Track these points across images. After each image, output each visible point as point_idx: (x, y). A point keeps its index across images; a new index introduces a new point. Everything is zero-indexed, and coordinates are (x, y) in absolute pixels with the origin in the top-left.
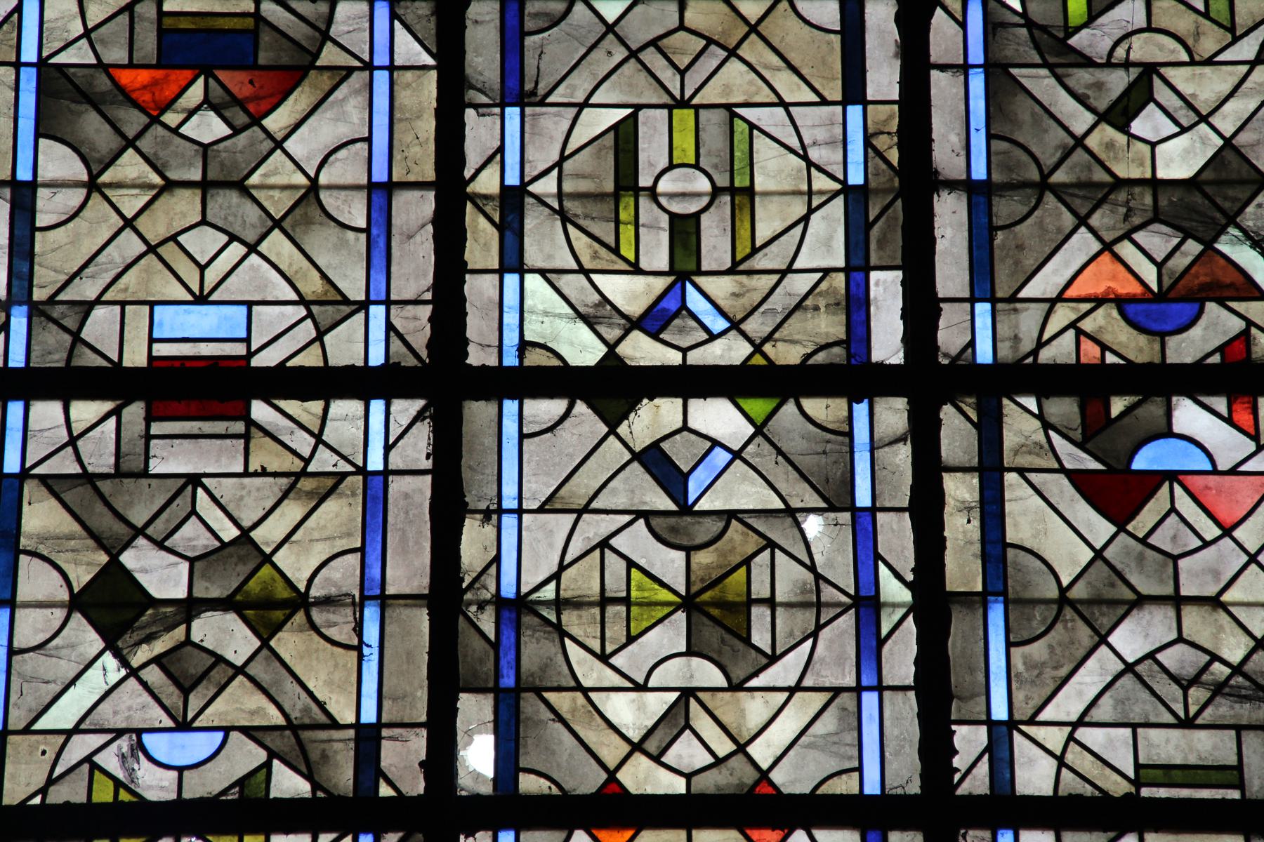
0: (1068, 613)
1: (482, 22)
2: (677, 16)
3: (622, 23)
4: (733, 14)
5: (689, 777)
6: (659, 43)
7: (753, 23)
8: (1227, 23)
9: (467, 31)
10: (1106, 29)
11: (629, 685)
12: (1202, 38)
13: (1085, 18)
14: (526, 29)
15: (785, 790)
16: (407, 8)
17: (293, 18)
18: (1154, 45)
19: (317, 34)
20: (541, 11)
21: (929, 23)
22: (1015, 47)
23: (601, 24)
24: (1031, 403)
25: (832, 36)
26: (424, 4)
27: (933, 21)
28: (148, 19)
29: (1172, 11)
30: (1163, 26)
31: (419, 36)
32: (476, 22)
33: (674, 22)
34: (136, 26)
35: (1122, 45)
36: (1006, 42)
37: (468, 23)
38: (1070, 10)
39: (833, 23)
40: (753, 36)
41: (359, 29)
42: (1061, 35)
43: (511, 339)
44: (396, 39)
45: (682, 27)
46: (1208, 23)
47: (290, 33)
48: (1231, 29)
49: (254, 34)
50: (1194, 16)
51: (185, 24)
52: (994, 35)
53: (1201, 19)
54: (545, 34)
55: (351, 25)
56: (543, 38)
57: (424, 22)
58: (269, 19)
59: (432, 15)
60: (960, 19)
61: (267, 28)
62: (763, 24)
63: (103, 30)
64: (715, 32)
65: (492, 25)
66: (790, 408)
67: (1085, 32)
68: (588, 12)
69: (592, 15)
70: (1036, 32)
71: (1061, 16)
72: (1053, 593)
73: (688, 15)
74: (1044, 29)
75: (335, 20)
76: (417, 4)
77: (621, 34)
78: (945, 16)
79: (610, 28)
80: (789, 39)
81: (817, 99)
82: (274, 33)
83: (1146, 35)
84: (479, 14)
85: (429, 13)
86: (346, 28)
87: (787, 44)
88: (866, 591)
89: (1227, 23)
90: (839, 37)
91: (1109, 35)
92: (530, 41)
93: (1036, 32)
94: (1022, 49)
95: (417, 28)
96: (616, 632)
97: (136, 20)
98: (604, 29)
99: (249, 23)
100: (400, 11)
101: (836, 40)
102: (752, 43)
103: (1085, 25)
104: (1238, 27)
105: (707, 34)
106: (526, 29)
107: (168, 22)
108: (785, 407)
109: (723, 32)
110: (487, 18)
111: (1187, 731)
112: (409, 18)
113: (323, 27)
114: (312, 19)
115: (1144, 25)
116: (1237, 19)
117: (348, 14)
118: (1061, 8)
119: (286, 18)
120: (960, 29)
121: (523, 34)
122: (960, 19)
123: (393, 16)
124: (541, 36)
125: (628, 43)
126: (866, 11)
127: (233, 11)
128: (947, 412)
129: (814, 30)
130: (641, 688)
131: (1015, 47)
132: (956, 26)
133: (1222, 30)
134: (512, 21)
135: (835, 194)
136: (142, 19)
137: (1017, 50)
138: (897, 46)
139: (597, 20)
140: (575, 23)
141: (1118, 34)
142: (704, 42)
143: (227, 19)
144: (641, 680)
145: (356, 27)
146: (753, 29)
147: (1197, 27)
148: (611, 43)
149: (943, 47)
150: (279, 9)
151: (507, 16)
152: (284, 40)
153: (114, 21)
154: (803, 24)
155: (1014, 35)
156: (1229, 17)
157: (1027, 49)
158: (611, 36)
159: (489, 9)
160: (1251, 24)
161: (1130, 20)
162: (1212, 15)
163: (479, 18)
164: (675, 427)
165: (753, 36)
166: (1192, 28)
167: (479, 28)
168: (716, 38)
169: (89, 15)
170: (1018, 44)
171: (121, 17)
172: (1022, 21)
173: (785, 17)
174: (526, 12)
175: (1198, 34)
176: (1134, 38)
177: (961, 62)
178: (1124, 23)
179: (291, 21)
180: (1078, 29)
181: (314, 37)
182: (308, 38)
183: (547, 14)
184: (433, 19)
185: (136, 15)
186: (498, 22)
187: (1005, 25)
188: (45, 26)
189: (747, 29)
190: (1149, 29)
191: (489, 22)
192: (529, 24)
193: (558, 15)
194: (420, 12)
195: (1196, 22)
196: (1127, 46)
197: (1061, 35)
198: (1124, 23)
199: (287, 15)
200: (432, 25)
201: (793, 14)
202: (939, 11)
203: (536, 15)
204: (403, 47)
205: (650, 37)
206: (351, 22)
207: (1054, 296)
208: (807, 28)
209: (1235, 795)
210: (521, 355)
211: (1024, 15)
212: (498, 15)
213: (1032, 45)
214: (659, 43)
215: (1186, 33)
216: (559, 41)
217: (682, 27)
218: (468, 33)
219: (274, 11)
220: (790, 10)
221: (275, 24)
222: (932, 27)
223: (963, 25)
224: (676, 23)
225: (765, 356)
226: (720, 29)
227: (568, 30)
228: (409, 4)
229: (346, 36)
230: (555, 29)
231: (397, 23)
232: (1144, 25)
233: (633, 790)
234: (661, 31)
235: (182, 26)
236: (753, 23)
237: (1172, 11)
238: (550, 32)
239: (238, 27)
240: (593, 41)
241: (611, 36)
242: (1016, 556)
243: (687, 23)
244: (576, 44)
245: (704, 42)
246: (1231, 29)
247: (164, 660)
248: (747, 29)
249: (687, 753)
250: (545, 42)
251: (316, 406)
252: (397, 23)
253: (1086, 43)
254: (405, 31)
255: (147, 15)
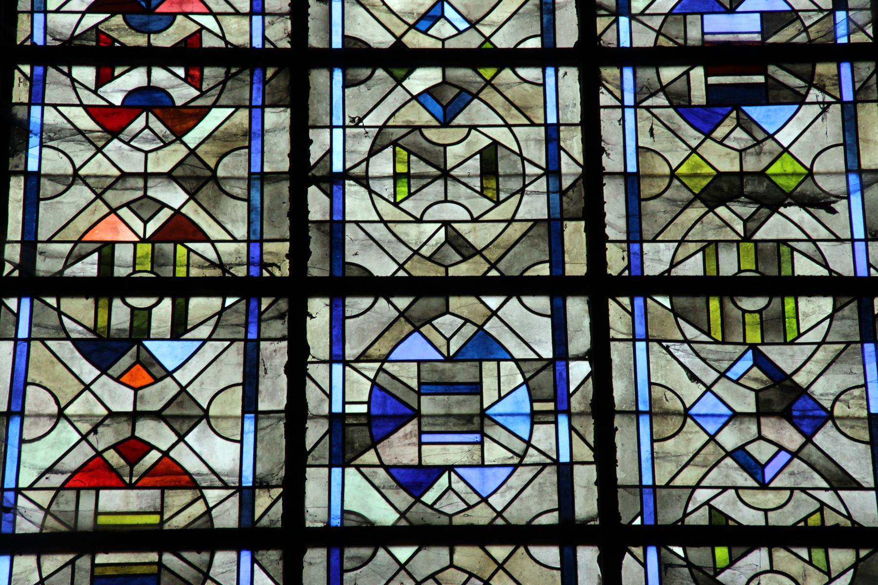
0: (676, 182)
1: (315, 564)
2: (448, 558)
3: (411, 562)
4: (487, 556)
5: (443, 41)
6: (436, 577)
7: (500, 562)
8: (825, 569)
9: (304, 570)
10: (742, 570)
11: (411, 219)
12: (808, 578)
13: (728, 562)
14: (345, 568)
15: (499, 46)
16: (263, 555)
17: (184, 564)
18: (776, 582)
19: (201, 575)
20: (355, 555)
21: (622, 564)
22: (681, 581)
23: (396, 564)
24: (666, 301)
25: (555, 572)
26: (274, 552)
27: (624, 562)
28: (84, 570)
29: (787, 559)
30: (781, 569)
31: (271, 574)
32: (310, 563)
33: (447, 562)
34: (76, 574)
35: (754, 581)
36: (674, 577)
37: (305, 564)
38: (717, 556)
39: (555, 563)
40: (501, 572)
41: (230, 570)
42: (712, 573)
43: (336, 511)
44: (255, 577)
45: (451, 565)
46: (812, 568)
47: (182, 575)
48: (828, 573)
49: (157, 577)
50: (802, 563)
51: (110, 572)
52: (666, 573)
53: (807, 565)
54: (358, 571)
55: (224, 568)
56: (356, 574)
57: (275, 564)
58: (168, 566)
59: (280, 559)
60: (642, 561)
61: (166, 572)
62: (507, 563)
63: (53, 578)
64: (474, 568)
65: (321, 565)
66: (514, 301)
67: (728, 572)
68: (387, 556)
69: (390, 557)
70: (695, 571)
71: (711, 560)
72: (667, 171)
73: (456, 557)
74: (700, 569)
75: (213, 565)
76: (270, 552)
77: (410, 570)
78: (632, 559)
79: (402, 567)
80: (525, 573)
81: (528, 122)
82: (171, 575)
83: (769, 575)
84: (313, 558)
85: (278, 558)
86: (221, 570)
87: (524, 577)
88: (552, 167)
89: (825, 569)
90: (559, 572)
91: (744, 574)
92: (347, 576)
93: (695, 571)
94: (685, 582)
95: (269, 569)
96: (403, 191)
97: (76, 570)
98: (398, 567)
99: (155, 569)
100: (258, 558)
101: (558, 574)
102: (500, 576)
103: (728, 567)
104: (832, 572)
105: (469, 570)
106: (345, 568)
107: (98, 571)
108: (511, 301)
109: (480, 569)
110: (318, 561)
111: (731, 16)
112: (265, 562)
113: (205, 570)
114: (198, 565)
115: (768, 568)
116: (831, 566)
117: (222, 561)
118: (711, 555)
119: (180, 564)
120: (642, 568)
121: (343, 571)
122: (642, 561)
123: (254, 561)
124: (355, 572)
125: (415, 576)
126: (578, 555)
127: (143, 561)
128: (612, 305)
129: (542, 567)
130: (419, 221)
131: (681, 581)
132: (640, 566)
133: (821, 574)
134: (335, 563)
135: (539, 177)
136: (80, 569)
137: (682, 583)
138: (600, 579)
139: (393, 561)
140: (378, 563)
141: (751, 573)
142: (467, 576)
143: (139, 567)
144: (419, 217)
145: (228, 569)
146: (501, 566)
147: (805, 571)
148: (403, 576)
149: (631, 580)
150: (175, 559)
151: (332, 559)
152: (178, 580)
153: (61, 572)
154: (534, 563)
155: (679, 572)
156: (826, 565)
157: (689, 582)
158: (403, 572)
159: (320, 555)
160: (841, 570)
161: (758, 564)
162: (814, 563)
163: (312, 561)
164: (445, 565)
165: (501, 572)
166: (801, 571)
167: (313, 568)
168: (475, 573)
169: (43, 569)
170: (682, 579)
171: (66, 568)
172: (685, 563)
173: (522, 558)
174: (345, 556)
175: (805, 575)
176: (762, 577)
177: (637, 483)
178: (755, 566)
179: (182, 566)
180: (723, 570)
181: (199, 577)
182: (194, 578)
183: (359, 558)
184: (281, 562)
185: (76, 567)
186: (325, 564)
187: (673, 566)
188: (13, 578)
189: (496, 566)
190: (772, 571)
191: (319, 563)
192: (347, 565)
193: (367, 558)
194: (272, 558)
195: (803, 567)
196: (757, 582)
197: (712, 573)
198: (755, 566)
199: (181, 562)
200: (280, 567)
201: (528, 556)
202: (627, 555)
203: (352, 558)
204: (260, 582)
205: (430, 572)
206: (224, 566)
207: (694, 485)
208: (538, 566)
209: (760, 79)
210: (342, 518)
211: (686, 559)
212: (326, 559)
213: (692, 580)
214: (436, 577)
215: (797, 574)
216: (367, 576)
217: (451, 565)
218: (305, 571)
219: (172, 561)
220: (525, 553)
221: (172, 569)
222: (623, 566)
223: (644, 565)
224: (448, 563)
225: (492, 43)
226: (478, 567)
227: (373, 568)
228: (264, 552)
229: (220, 576)
230: (365, 568)
231: (256, 566)
232: (768, 568)
233: (410, 46)
234: (438, 569)
235: (108, 573)
236: (500, 562)
237: (787, 559)
238: (361, 570)
239: (147, 572)
240: (391, 575)
241: (403, 572)
242: (662, 447)
243: (455, 562)
244: (379, 577)
245: (467, 576)
246: (828, 573)
247: (118, 447)
248: (496, 566)
249: (442, 29)
250: (358, 577)
251: (205, 556)
252: (256, 566)
253: (729, 579)
254: (261, 571)
255: (84, 567)
